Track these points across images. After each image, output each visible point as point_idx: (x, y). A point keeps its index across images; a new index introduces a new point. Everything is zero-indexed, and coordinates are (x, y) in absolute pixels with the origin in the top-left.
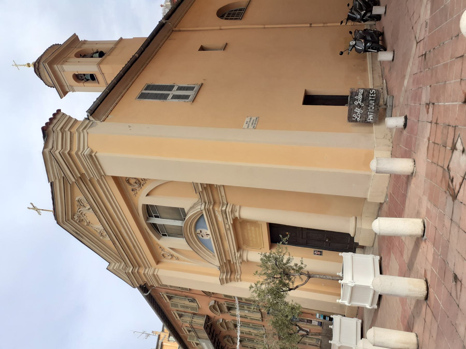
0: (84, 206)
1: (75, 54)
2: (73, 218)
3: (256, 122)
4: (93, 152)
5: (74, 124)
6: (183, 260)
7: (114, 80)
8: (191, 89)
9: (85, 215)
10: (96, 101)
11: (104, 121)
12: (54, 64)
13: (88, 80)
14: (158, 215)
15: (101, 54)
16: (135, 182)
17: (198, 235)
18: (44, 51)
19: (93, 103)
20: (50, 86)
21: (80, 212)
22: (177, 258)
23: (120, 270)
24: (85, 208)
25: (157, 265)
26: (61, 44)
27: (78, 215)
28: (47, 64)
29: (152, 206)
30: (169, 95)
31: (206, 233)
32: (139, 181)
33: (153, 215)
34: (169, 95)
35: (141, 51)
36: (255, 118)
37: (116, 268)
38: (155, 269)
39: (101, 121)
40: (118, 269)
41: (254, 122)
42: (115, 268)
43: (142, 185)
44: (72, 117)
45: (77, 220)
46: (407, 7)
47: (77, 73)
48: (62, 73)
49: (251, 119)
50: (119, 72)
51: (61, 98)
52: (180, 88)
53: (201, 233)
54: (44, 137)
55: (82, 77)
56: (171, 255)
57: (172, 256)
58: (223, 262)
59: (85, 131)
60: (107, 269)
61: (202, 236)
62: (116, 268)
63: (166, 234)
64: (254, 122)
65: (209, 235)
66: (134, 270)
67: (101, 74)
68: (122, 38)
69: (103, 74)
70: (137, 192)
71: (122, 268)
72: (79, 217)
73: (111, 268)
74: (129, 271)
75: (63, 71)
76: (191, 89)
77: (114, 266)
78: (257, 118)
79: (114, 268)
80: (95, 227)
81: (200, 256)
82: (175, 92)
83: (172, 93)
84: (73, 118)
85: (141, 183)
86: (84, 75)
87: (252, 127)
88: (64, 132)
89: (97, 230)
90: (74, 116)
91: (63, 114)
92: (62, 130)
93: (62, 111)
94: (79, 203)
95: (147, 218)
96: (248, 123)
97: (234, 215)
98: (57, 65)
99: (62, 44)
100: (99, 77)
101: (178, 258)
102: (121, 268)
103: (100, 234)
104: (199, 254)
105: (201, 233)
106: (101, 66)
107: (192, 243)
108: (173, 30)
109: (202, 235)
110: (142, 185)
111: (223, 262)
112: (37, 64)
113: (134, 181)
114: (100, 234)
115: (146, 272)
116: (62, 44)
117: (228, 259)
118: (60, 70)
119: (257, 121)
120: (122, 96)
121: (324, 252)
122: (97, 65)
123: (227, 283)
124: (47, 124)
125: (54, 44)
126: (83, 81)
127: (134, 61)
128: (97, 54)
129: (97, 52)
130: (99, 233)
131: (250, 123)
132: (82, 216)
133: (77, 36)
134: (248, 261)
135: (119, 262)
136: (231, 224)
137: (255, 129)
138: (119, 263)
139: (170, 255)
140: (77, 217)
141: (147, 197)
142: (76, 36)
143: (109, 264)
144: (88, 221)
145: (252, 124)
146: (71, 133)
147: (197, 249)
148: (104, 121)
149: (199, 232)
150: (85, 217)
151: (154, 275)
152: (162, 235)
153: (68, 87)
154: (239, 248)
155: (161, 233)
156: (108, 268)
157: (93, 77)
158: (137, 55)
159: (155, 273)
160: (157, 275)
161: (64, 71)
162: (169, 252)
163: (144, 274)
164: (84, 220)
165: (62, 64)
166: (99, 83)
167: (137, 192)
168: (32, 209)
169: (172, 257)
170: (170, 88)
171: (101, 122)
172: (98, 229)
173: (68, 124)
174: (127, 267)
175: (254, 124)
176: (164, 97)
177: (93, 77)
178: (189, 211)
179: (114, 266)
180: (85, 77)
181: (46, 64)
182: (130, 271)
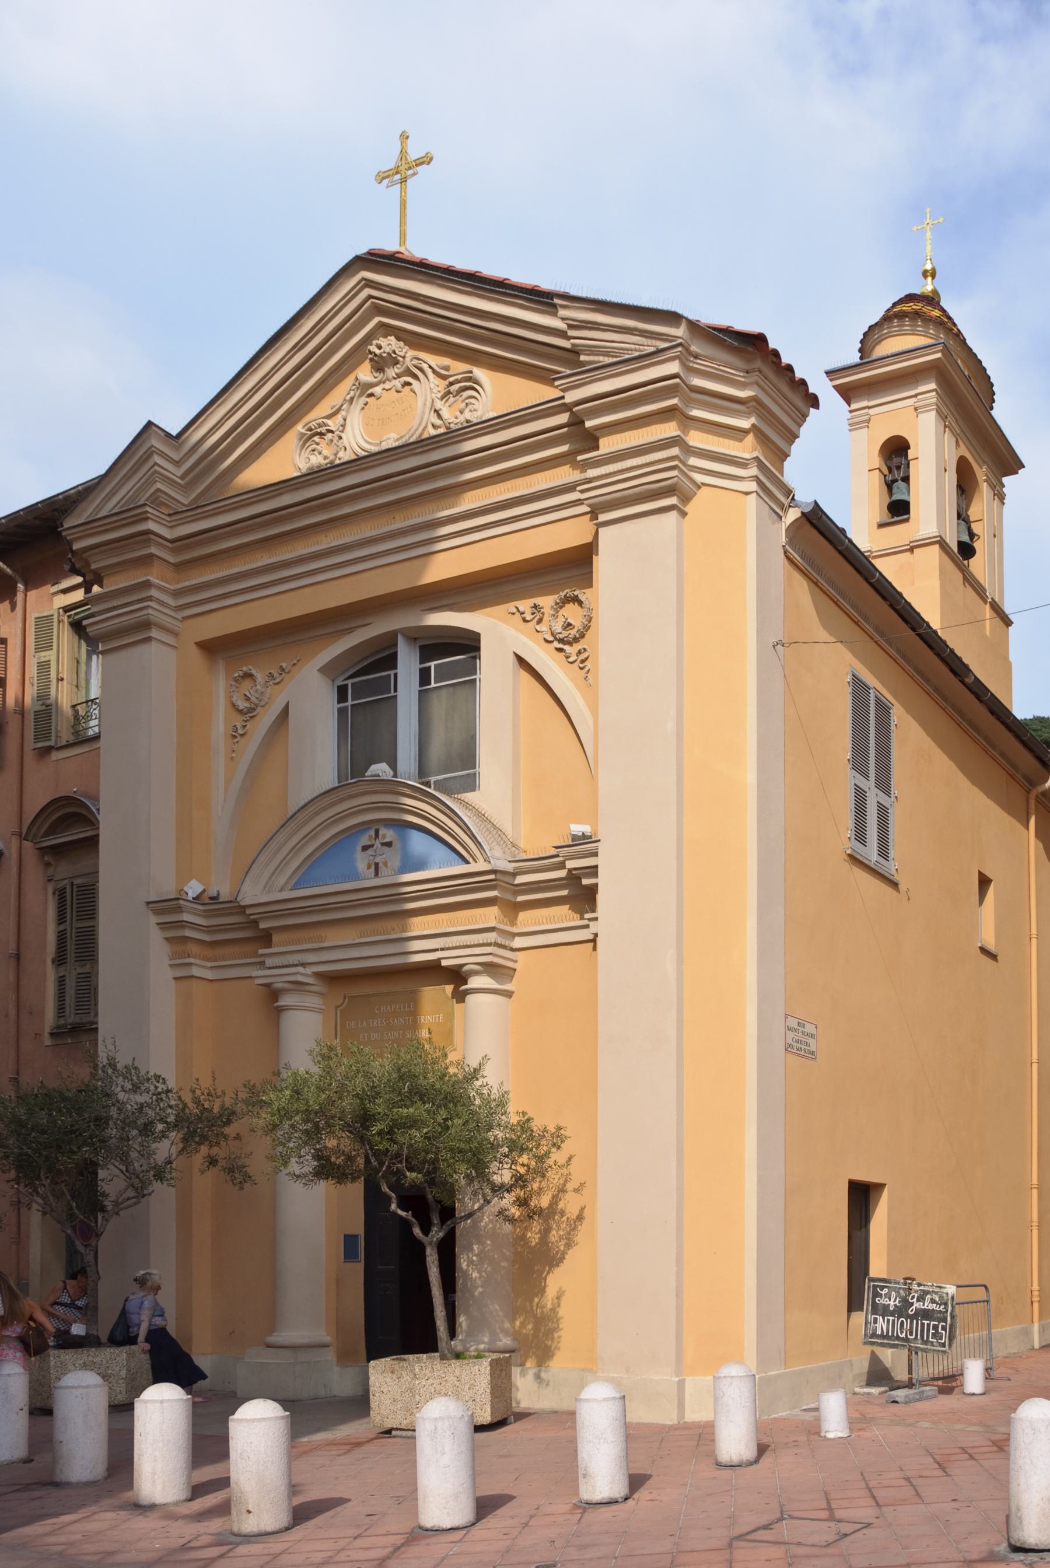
0: (449, 393)
1: (967, 459)
2: (386, 330)
3: (802, 1053)
4: (683, 501)
5: (770, 445)
6: (234, 755)
7: (906, 601)
8: (884, 852)
9: (407, 388)
10: (846, 537)
11: (785, 552)
12: (938, 384)
13: (890, 486)
14: (433, 685)
15: (967, 550)
16: (570, 624)
17: (372, 833)
18: (974, 351)
19: (840, 525)
20: (864, 337)
21: (416, 367)
22: (240, 732)
23: (150, 482)
24: (439, 395)
25: (194, 645)
26: (992, 408)
27: (404, 357)
28: (939, 359)
29: (471, 667)
30: (866, 776)
31: (385, 864)
32: (576, 640)
33: (432, 664)
34: (866, 776)
35: (979, 691)
36: (813, 1048)
37: (156, 464)
38: (175, 634)
39: (787, 547)
40: (156, 472)
41: (803, 1047)
42: (157, 459)
43: (561, 646)
44: (793, 442)
45: (380, 347)
46: (88, 1516)
47: (911, 454)
48: (911, 401)
49: (812, 1036)
50: (926, 620)
51: (828, 373)
52: (883, 813)
53: (383, 844)
54: (728, 331)
55: (898, 468)
56: (251, 710)
57: (249, 713)
58: (262, 918)
59: (753, 486)
60: (150, 424)
61: (365, 848)
62: (159, 462)
63: (350, 702)
64: (803, 1047)
65: (377, 874)
66: (160, 545)
67: (911, 542)
68: (1011, 626)
69: (911, 550)
70: (528, 621)
71: (158, 490)
72: (392, 360)
73: (155, 442)
74: (152, 519)
75: (917, 405)
76: (884, 852)
77: (163, 455)
78: (813, 1053)
79: (157, 459)
80: (348, 411)
81: (274, 831)
82: (874, 797)
83: (869, 785)
84: (791, 445)
85: (570, 644)
86: (906, 479)
87: (790, 1041)
88: (748, 408)
89: (339, 418)
90: (796, 447)
91: (805, 416)
92: (754, 403)
93: (812, 410)
94: (460, 377)
95: (415, 639)
96: (801, 1029)
97: (476, 973)
98: (935, 390)
99: (992, 412)
100: (900, 534)
101: (241, 735)
102: (159, 485)
103: (320, 426)
104: (283, 826)
105: (383, 844)
106: (937, 546)
107: (333, 804)
108: (1029, 793)
109: (372, 846)
110: (561, 646)
111: (262, 918)
112: (936, 313)
113: (577, 622)
114: (320, 426)
115: (154, 592)
116: (992, 412)
117: (276, 938)
118: (919, 397)
119: (807, 1055)
120: (856, 623)
121: (357, 1270)
122: (940, 536)
123: (158, 924)
124: (776, 354)
125: (994, 388)
126: (885, 471)
127: (957, 668)
128: (966, 538)
129: (972, 535)
130: (325, 425)
131: (800, 1034)
132: (397, 371)
133: (1017, 473)
134: (280, 1010)
135: (188, 479)
136: (439, 960)
137: (786, 1050)
138: (182, 477)
139: (253, 706)
140: (394, 352)
141: (512, 659)
142: (1015, 466)
143: (174, 433)
144: (377, 390)
145: (798, 1041)
146: (746, 432)
147: (305, 823)
148: (787, 557)
149: (384, 836)
150: (398, 383)
151: (146, 625)
152: (340, 682)
153: (866, 410)
154: (332, 979)
155: (349, 682)
156: (154, 428)
157: (899, 510)
158: (969, 680)
159: (154, 633)
160: (149, 639)
161: (916, 409)
162: (263, 703)
163: (147, 585)
164: (380, 376)
165: (939, 412)
166: (881, 525)
167: (528, 621)
168: (403, 153)
169: (240, 712)
170: (884, 784)
171: (783, 546)
172: (342, 426)
173: (772, 427)
174: (169, 515)
175: (799, 1045)
176: (859, 764)
177: (899, 510)
178: (467, 805)
179: (163, 455)
180: (900, 481)
181: (939, 355)
182: (151, 526)
